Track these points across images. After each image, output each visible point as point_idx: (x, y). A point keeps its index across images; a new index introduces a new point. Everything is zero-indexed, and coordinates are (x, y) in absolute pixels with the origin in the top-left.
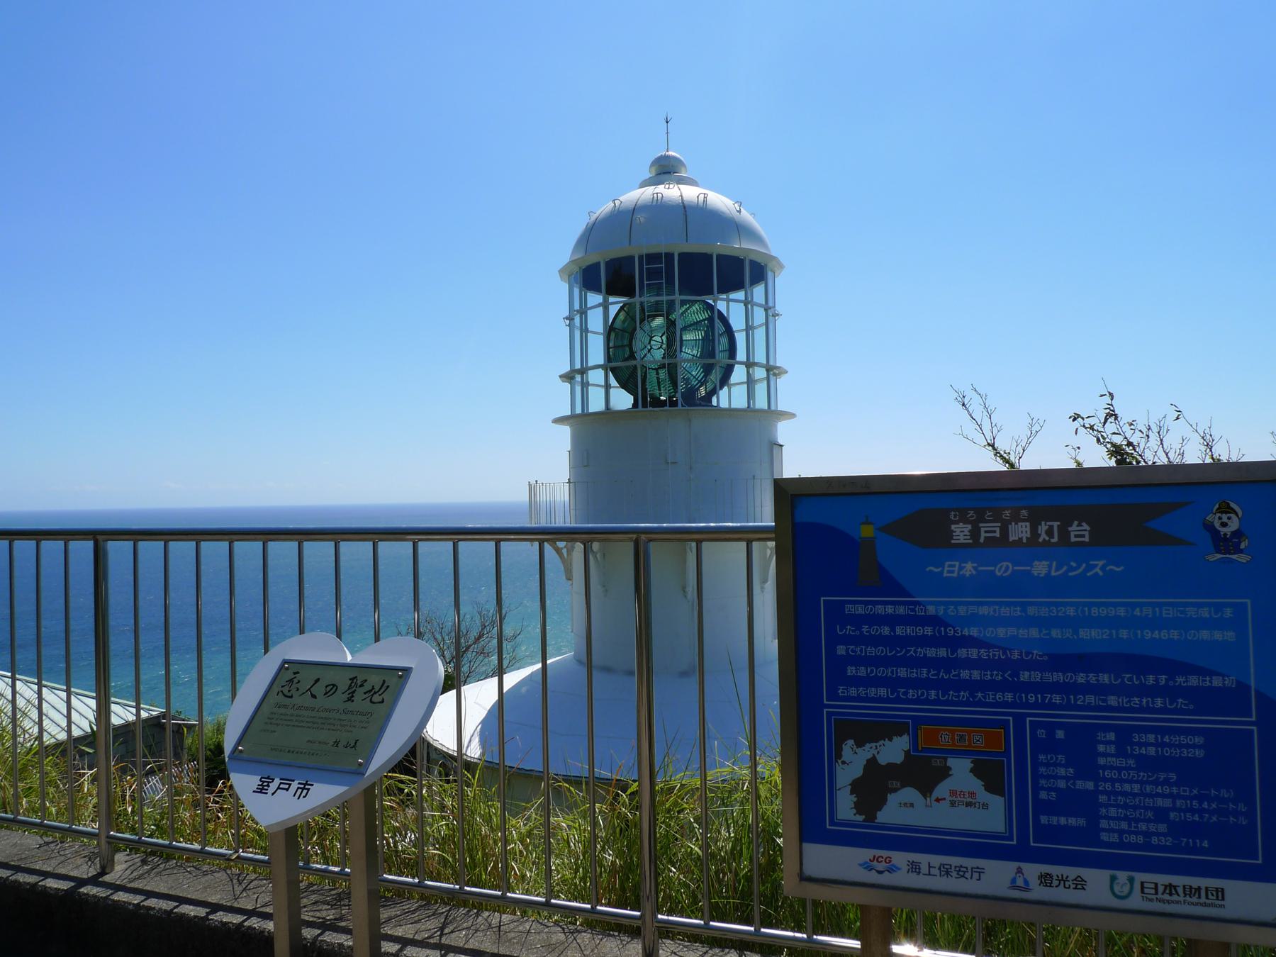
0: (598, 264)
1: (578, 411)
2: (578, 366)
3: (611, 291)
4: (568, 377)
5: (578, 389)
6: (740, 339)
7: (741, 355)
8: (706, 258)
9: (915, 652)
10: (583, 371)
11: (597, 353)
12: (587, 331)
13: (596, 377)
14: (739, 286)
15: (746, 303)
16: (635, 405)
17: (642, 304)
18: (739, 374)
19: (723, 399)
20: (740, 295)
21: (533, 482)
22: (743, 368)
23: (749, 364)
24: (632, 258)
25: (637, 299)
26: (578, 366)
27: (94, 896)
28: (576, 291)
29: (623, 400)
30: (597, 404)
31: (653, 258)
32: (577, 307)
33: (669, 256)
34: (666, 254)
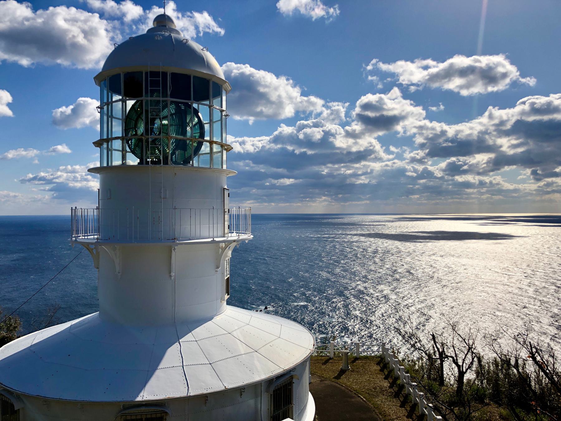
0: (119, 75)
1: (105, 165)
2: (105, 137)
3: (128, 95)
4: (98, 144)
5: (105, 151)
6: (207, 127)
7: (207, 138)
8: (188, 77)
9: (520, 412)
10: (109, 140)
11: (118, 129)
12: (112, 117)
13: (117, 144)
14: (207, 98)
15: (210, 106)
16: (141, 163)
17: (147, 101)
18: (205, 148)
19: (195, 162)
20: (207, 102)
21: (74, 208)
22: (208, 144)
23: (211, 142)
24: (142, 73)
25: (143, 98)
26: (105, 137)
27: (534, 120)
28: (105, 92)
29: (133, 161)
30: (117, 162)
31: (154, 74)
32: (105, 101)
33: (165, 74)
34: (163, 73)
